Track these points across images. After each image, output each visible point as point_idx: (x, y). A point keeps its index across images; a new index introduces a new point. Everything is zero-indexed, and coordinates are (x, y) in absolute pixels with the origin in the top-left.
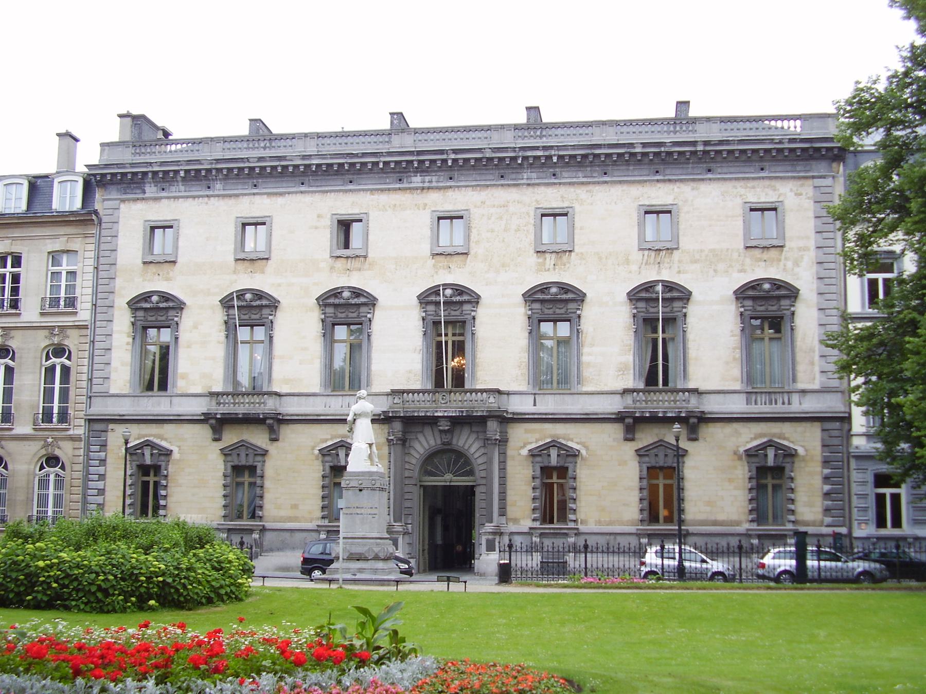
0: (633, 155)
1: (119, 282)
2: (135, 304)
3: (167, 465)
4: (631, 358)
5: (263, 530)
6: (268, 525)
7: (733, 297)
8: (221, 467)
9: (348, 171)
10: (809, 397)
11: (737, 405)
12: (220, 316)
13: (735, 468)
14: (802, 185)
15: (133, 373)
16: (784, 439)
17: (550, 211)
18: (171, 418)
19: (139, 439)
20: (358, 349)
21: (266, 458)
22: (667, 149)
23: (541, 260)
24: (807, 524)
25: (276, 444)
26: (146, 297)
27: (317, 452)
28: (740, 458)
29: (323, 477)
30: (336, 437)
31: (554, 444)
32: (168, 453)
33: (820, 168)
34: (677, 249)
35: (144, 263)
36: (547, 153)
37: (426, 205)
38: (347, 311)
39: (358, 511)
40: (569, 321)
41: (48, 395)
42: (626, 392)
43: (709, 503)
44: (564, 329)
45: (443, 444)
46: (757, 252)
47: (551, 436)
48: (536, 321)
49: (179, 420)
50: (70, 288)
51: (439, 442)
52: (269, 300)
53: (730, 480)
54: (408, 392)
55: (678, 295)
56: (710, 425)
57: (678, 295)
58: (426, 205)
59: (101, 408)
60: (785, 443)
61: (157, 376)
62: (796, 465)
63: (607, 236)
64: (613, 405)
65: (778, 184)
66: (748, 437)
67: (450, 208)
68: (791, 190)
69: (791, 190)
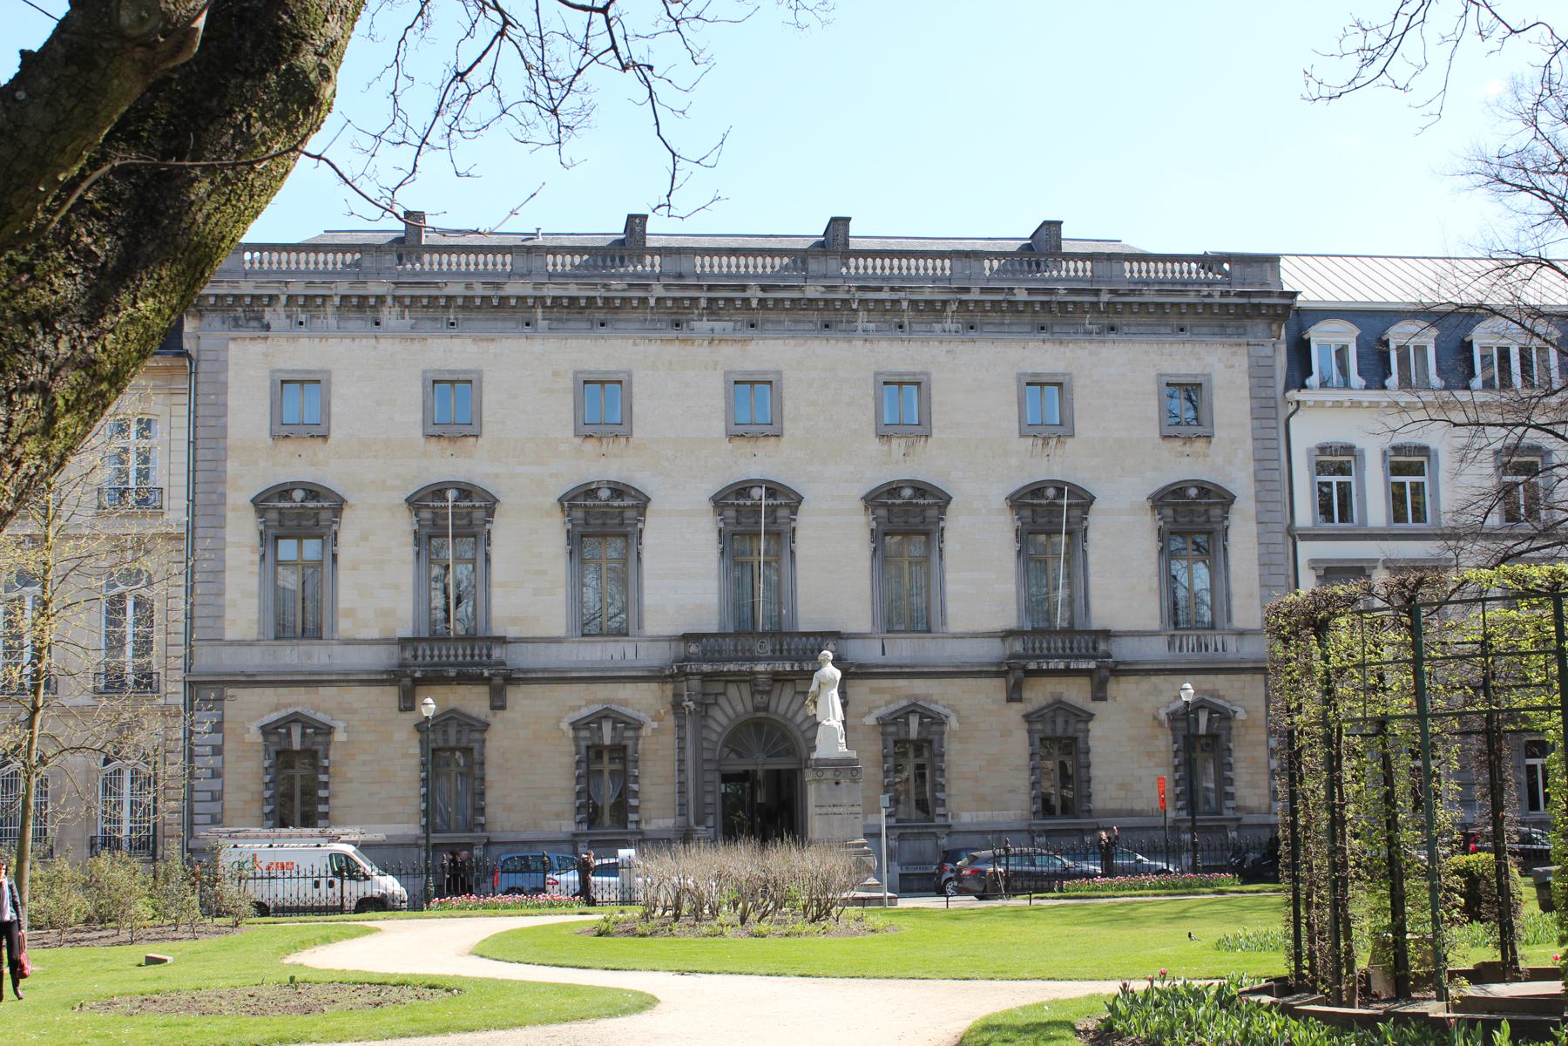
0: (746, 301)
1: (231, 466)
2: (261, 503)
3: (327, 750)
4: (1013, 588)
5: (489, 843)
6: (495, 837)
7: (1148, 505)
8: (415, 750)
9: (479, 307)
10: (1248, 640)
11: (1156, 650)
12: (404, 524)
13: (1156, 737)
14: (1235, 354)
15: (262, 610)
16: (1219, 697)
17: (897, 379)
18: (296, 678)
19: (277, 709)
20: (627, 575)
21: (487, 736)
22: (1060, 299)
23: (886, 448)
24: (1250, 811)
25: (500, 714)
26: (284, 491)
27: (565, 726)
28: (1161, 725)
29: (885, 756)
30: (593, 702)
31: (913, 709)
32: (328, 730)
33: (1260, 327)
34: (1072, 436)
35: (273, 437)
36: (894, 296)
37: (716, 363)
38: (603, 521)
39: (835, 810)
40: (321, 537)
41: (115, 644)
42: (1008, 634)
43: (1123, 786)
44: (312, 548)
45: (757, 709)
46: (1177, 444)
47: (604, 701)
48: (424, 539)
49: (345, 679)
50: (143, 475)
51: (750, 708)
52: (788, 497)
53: (1150, 755)
54: (705, 635)
55: (784, 499)
56: (1122, 679)
57: (784, 499)
58: (716, 363)
59: (207, 659)
60: (1220, 702)
61: (300, 616)
62: (1234, 732)
63: (977, 413)
64: (993, 651)
65: (1201, 349)
66: (581, 701)
67: (299, 365)
68: (1220, 360)
69: (1220, 360)
